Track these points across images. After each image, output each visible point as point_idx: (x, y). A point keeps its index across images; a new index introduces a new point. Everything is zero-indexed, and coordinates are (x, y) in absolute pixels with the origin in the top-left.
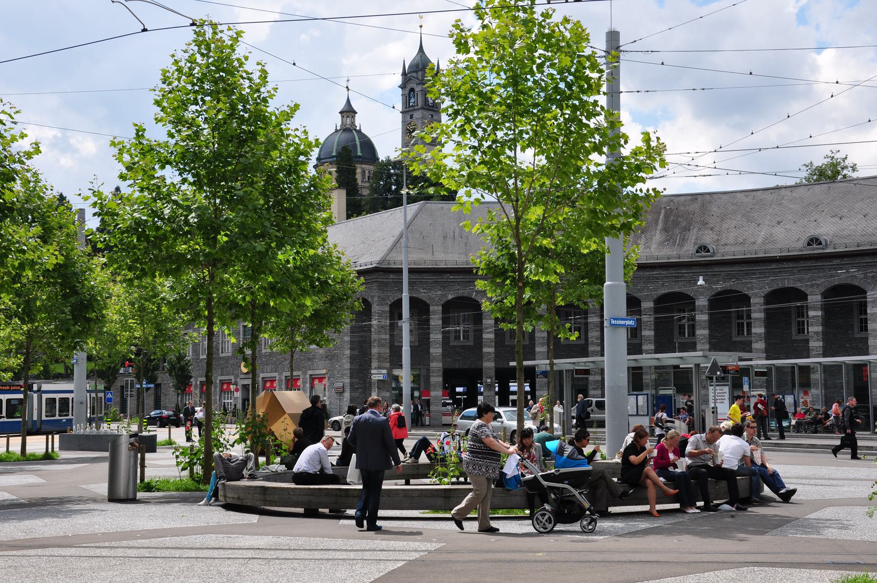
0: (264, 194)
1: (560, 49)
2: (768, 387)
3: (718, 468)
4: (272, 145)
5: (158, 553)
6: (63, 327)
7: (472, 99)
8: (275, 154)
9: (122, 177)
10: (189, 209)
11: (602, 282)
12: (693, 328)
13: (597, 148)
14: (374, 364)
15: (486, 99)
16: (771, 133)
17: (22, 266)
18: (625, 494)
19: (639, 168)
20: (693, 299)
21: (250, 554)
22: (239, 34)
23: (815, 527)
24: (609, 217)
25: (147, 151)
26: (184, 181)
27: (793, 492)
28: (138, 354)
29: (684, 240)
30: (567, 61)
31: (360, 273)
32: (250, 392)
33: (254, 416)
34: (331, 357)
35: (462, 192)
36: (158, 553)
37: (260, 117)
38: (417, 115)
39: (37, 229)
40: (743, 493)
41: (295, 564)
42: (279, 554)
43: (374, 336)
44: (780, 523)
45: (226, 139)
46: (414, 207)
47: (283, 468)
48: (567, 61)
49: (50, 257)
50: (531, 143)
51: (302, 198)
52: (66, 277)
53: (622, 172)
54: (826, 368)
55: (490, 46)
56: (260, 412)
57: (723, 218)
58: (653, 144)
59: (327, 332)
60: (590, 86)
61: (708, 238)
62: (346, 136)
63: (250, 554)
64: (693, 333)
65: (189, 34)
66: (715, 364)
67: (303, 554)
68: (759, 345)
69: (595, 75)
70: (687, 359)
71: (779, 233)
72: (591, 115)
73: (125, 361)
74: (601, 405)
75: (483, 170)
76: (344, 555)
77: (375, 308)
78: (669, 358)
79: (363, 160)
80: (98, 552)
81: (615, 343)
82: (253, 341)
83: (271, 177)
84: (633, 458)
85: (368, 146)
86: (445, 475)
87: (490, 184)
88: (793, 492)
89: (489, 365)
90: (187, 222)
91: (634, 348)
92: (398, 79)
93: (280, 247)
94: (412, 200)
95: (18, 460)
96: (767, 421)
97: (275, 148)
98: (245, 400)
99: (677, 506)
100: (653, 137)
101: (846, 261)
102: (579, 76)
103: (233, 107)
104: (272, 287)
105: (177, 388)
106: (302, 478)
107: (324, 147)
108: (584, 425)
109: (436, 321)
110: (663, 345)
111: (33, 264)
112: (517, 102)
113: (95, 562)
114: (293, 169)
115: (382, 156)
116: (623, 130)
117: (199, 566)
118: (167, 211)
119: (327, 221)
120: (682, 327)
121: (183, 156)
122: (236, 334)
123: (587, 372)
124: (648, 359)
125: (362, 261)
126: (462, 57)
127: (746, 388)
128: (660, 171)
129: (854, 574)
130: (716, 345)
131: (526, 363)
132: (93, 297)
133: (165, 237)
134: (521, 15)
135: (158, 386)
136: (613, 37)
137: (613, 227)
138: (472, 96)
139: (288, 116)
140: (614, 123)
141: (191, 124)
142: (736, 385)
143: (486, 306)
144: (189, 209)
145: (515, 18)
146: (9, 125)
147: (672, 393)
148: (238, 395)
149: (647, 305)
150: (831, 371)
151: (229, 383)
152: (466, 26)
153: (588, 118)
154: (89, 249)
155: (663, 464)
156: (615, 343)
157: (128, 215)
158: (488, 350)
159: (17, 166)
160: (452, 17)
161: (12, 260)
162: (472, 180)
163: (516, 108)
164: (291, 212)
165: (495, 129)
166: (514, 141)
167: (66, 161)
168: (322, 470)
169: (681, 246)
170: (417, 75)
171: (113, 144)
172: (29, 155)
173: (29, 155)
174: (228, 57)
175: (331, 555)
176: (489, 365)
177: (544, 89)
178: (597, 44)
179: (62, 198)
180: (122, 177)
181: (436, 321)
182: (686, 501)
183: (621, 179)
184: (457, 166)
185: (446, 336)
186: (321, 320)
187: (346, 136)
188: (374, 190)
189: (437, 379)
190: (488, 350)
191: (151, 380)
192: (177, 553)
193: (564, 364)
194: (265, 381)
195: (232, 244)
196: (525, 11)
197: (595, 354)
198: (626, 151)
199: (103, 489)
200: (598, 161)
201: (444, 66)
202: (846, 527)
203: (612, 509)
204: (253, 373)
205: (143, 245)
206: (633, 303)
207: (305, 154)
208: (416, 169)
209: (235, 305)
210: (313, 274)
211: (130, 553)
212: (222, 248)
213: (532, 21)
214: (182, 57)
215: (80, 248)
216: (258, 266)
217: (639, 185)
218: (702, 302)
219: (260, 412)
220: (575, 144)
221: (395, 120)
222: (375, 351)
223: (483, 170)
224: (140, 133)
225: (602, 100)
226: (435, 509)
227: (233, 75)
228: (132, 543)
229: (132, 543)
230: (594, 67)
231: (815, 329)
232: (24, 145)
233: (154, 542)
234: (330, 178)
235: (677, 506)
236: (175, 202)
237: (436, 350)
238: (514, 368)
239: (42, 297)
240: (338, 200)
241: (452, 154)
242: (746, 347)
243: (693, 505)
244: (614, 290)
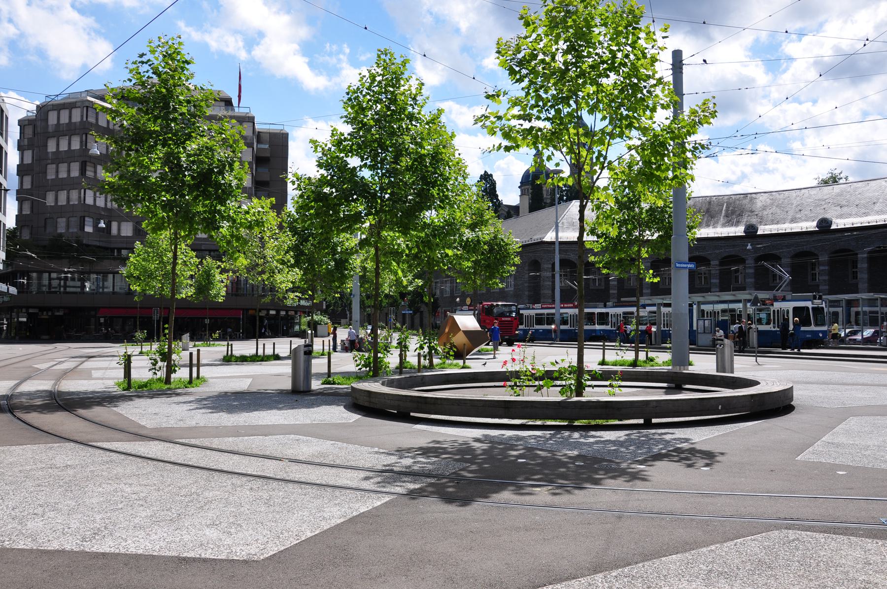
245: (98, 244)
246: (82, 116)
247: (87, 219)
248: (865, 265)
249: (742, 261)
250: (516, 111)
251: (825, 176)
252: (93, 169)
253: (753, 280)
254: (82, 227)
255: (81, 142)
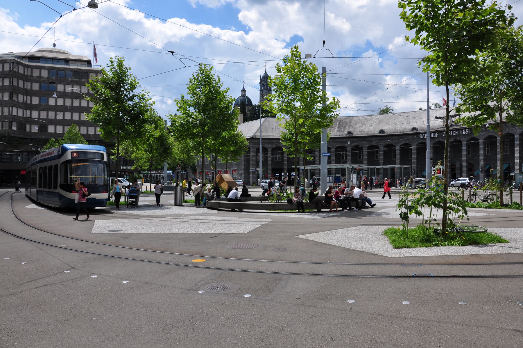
0: (219, 115)
1: (309, 72)
2: (368, 175)
3: (353, 198)
4: (221, 100)
5: (190, 221)
6: (161, 155)
7: (282, 87)
8: (222, 103)
9: (178, 110)
10: (197, 120)
11: (320, 142)
12: (346, 157)
13: (320, 102)
14: (251, 167)
15: (286, 87)
16: (372, 99)
17: (150, 137)
18: (326, 206)
19: (332, 108)
20: (345, 147)
21: (216, 222)
22: (212, 67)
23: (380, 214)
24: (323, 122)
25: (185, 102)
26: (195, 111)
27: (375, 204)
28: (182, 163)
29: (344, 130)
30: (311, 76)
31: (248, 139)
32: (214, 175)
33: (216, 181)
34: (238, 164)
35: (278, 115)
36: (190, 221)
37: (218, 92)
38: (265, 91)
39: (154, 126)
40: (360, 205)
41: (229, 225)
42: (224, 222)
43: (251, 158)
44: (370, 214)
45: (207, 99)
46: (263, 120)
47: (224, 197)
48: (311, 76)
49: (157, 134)
50: (299, 100)
51: (230, 116)
52: (162, 140)
53: (326, 109)
54: (384, 169)
55: (288, 71)
56: (217, 181)
57: (356, 124)
58: (336, 101)
59: (237, 157)
60: (317, 84)
61: (351, 130)
62: (242, 98)
63: (216, 222)
64: (346, 158)
65: (198, 68)
66: (353, 167)
67: (231, 222)
68: (365, 162)
69: (319, 80)
70: (346, 166)
71: (372, 128)
72: (318, 92)
73: (178, 165)
74: (319, 180)
75: (285, 108)
76: (243, 223)
77: (251, 150)
78: (339, 166)
79: (248, 105)
80: (173, 220)
81: (324, 160)
82: (215, 159)
83: (221, 110)
84: (329, 195)
85: (249, 101)
86: (273, 200)
87: (287, 112)
88: (375, 204)
89: (285, 167)
90: (196, 124)
91: (329, 163)
92: (259, 81)
93: (223, 131)
94: (263, 117)
95: (149, 194)
96: (367, 185)
97: (222, 101)
98: (213, 177)
99: (341, 209)
100: (336, 99)
101: (390, 137)
102: (314, 80)
103: (210, 89)
104: (221, 143)
105: (193, 173)
106: (230, 200)
107: (237, 101)
108: (315, 185)
109: (270, 154)
110: (338, 162)
111: (153, 136)
112: (296, 88)
113: (172, 222)
114: (227, 108)
115: (254, 104)
116: (327, 96)
117: (201, 224)
118: (190, 120)
119: (238, 123)
120: (343, 157)
121: (195, 104)
122: (210, 157)
123: (315, 169)
124: (333, 166)
125: (247, 135)
126: (279, 74)
127: (361, 174)
128: (338, 109)
129: (390, 227)
130: (354, 161)
131: (297, 167)
132: (169, 146)
133: (190, 128)
134: (297, 62)
135: (187, 173)
136: (324, 69)
137: (324, 125)
138: (282, 86)
139: (226, 92)
140: (324, 95)
141: (197, 94)
142: (359, 174)
143: (284, 150)
144: (197, 120)
145: (295, 63)
146: (147, 96)
147: (340, 176)
148: (210, 175)
149: (333, 150)
150: (385, 170)
151: (208, 172)
152: (280, 65)
153: (317, 93)
154: (168, 131)
155: (337, 197)
156: (324, 160)
157: (179, 121)
158: (285, 163)
159: (149, 108)
160: (276, 62)
161: (147, 135)
162: (281, 111)
163: (295, 89)
164: (227, 120)
165: (289, 96)
166: (295, 99)
167: (163, 106)
168: (236, 198)
169: (343, 132)
170: (265, 80)
171: (175, 101)
172: (152, 105)
173: (152, 105)
174: (209, 75)
175: (239, 222)
176: (285, 167)
177: (304, 84)
178: (319, 71)
179: (160, 117)
180: (178, 110)
181: (270, 154)
182: (344, 208)
183: (327, 111)
184: (277, 107)
185: (273, 158)
186: (235, 153)
187: (242, 98)
188: (251, 114)
189: (270, 171)
190: (285, 163)
191: (185, 170)
192: (195, 221)
193: (308, 167)
194: (218, 171)
195: (209, 131)
196: (298, 60)
197: (317, 164)
198: (328, 103)
199: (173, 202)
200: (319, 105)
201: (273, 77)
202: (388, 214)
203: (322, 210)
204: (215, 169)
205: (184, 130)
206: (329, 149)
207: (231, 103)
208: (265, 108)
209: (209, 149)
210: (234, 139)
211: (182, 220)
212: (206, 132)
213: (300, 64)
214: (195, 75)
215: (166, 132)
216: (217, 136)
217: (332, 113)
218: (349, 149)
219: (217, 181)
220: (313, 100)
221: (258, 93)
222: (251, 163)
223: (285, 108)
224: (183, 97)
225: (321, 87)
226: (270, 210)
227: (210, 80)
228: (182, 217)
229: (182, 217)
230: (319, 78)
231: (381, 157)
232: (151, 101)
233: (188, 217)
234: (238, 111)
235: (341, 209)
236: (193, 118)
237: (270, 163)
238: (293, 168)
239: (155, 146)
240: (240, 117)
241: (275, 103)
242: (362, 162)
243: (346, 209)
244: (324, 145)
245: (19, 136)
246: (10, 68)
247: (13, 123)
248: (399, 152)
249: (346, 150)
250: (133, 78)
251: (383, 108)
252: (16, 96)
253: (383, 157)
254: (11, 127)
255: (10, 82)
